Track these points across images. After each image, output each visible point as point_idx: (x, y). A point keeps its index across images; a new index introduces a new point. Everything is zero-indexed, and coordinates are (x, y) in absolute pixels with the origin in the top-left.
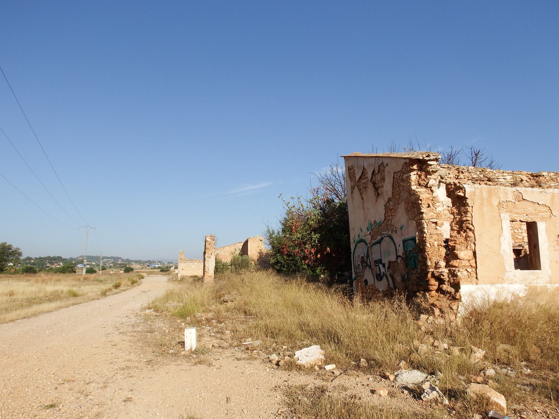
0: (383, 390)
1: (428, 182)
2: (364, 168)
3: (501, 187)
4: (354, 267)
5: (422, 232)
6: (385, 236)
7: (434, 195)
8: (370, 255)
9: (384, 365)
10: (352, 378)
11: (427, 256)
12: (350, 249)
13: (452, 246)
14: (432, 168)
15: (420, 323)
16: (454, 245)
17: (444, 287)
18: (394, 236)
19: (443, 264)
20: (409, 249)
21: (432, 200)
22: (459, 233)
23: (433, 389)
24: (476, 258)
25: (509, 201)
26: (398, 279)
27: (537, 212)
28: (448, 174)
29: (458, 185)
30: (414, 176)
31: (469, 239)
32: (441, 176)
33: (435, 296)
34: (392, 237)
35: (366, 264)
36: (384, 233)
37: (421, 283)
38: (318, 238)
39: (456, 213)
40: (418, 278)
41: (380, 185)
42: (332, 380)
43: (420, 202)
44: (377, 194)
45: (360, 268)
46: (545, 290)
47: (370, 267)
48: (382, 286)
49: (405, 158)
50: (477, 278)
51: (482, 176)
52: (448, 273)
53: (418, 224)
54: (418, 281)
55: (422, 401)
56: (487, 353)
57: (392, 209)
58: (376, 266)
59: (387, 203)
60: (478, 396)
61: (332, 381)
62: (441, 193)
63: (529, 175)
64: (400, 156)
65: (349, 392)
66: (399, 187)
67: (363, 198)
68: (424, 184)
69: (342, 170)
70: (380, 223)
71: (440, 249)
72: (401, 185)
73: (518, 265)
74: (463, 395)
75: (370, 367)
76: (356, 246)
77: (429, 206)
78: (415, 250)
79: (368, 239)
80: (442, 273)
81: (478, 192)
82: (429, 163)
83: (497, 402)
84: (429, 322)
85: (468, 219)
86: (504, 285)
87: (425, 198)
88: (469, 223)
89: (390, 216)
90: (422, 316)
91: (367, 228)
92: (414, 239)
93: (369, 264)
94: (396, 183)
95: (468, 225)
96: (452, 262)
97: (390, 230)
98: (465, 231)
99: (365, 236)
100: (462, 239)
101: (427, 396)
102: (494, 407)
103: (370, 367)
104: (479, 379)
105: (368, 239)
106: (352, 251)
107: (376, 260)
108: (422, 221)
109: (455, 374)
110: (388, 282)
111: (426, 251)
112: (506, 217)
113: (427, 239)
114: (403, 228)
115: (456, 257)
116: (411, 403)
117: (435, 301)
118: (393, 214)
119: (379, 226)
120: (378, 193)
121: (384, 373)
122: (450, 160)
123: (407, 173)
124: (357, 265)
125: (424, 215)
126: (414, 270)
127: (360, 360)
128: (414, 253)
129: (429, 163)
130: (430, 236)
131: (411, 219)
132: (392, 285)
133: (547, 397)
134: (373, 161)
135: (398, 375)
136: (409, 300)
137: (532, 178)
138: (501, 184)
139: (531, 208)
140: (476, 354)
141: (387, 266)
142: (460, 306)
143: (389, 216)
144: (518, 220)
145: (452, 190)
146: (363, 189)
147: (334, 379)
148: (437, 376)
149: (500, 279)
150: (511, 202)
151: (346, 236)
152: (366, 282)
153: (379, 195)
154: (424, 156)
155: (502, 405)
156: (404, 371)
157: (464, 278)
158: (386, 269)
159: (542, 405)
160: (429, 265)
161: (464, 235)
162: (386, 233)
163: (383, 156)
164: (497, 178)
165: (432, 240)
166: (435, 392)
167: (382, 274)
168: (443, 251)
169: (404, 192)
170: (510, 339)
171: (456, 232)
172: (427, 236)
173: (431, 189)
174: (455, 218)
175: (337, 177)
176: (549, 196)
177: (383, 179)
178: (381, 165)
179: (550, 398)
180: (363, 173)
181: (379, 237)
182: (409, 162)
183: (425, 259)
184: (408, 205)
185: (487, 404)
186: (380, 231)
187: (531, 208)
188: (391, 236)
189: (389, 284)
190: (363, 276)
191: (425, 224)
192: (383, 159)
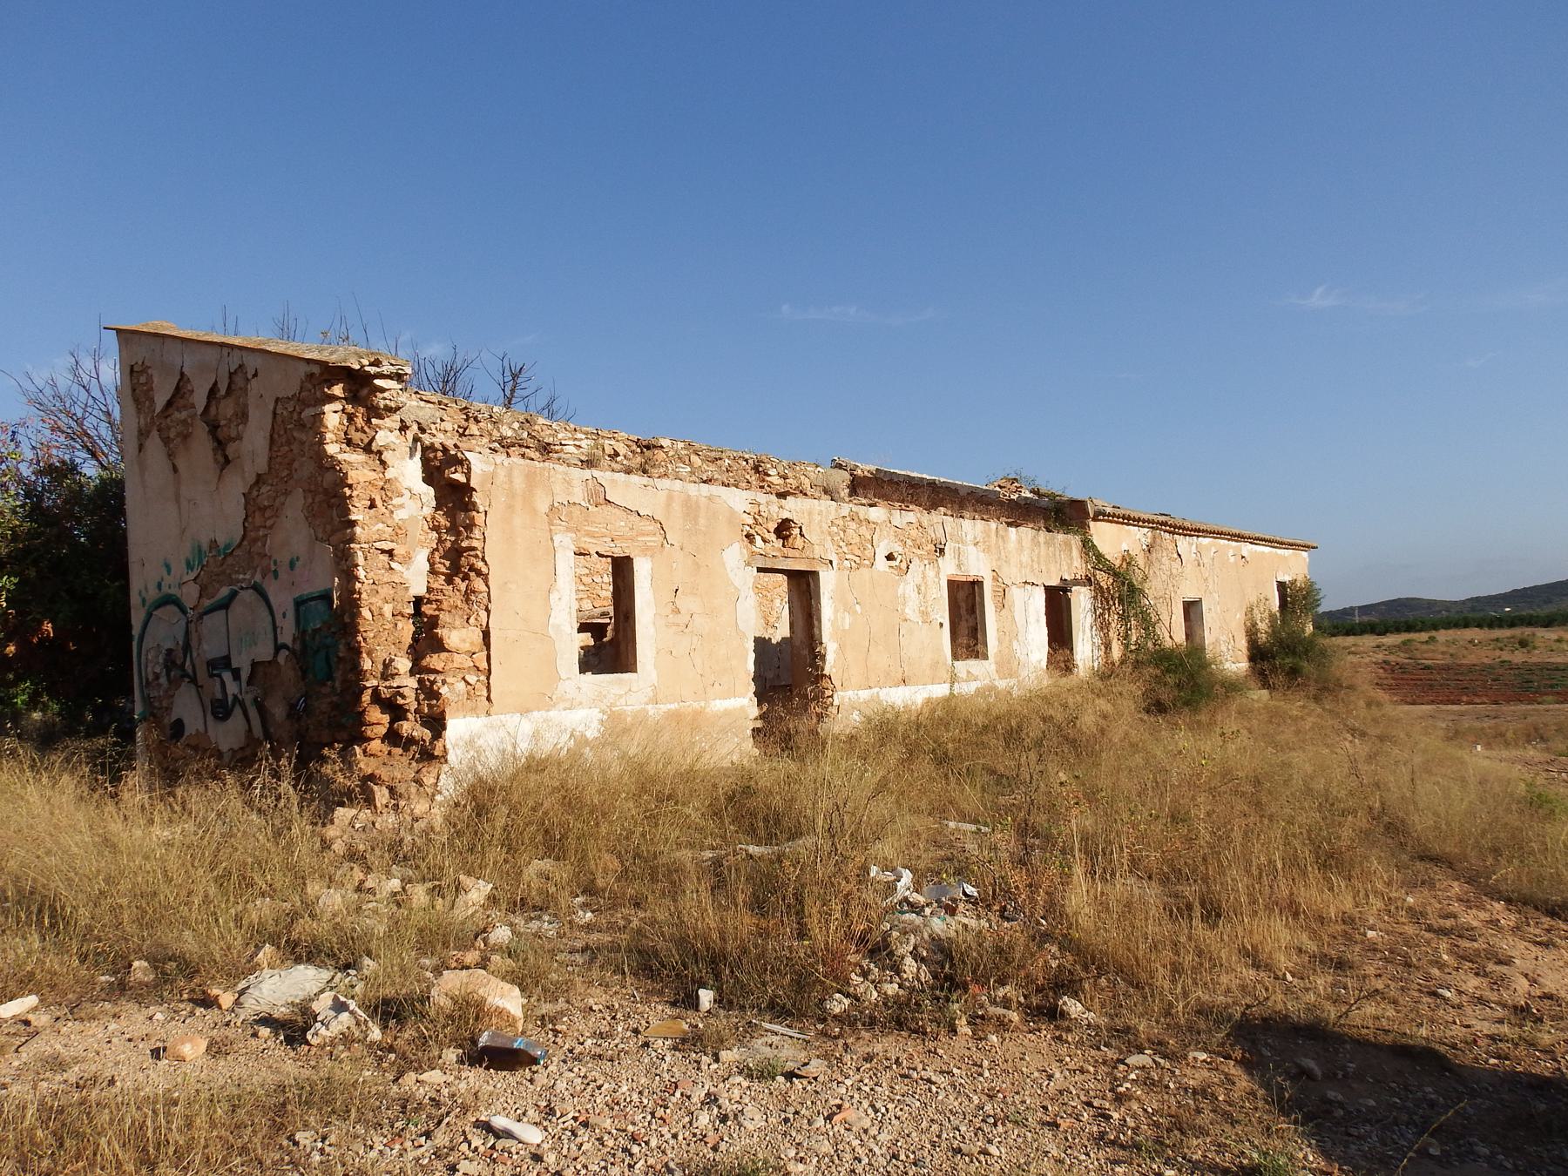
0: (191, 1041)
1: (374, 438)
2: (182, 374)
3: (557, 466)
4: (141, 683)
5: (349, 576)
6: (242, 588)
7: (390, 474)
8: (194, 643)
9: (204, 966)
10: (93, 1028)
11: (363, 644)
12: (130, 627)
13: (431, 616)
14: (385, 399)
15: (331, 832)
16: (437, 613)
17: (405, 727)
18: (272, 589)
19: (403, 664)
20: (311, 627)
21: (382, 489)
22: (449, 581)
23: (339, 1007)
24: (488, 649)
25: (574, 503)
26: (278, 711)
27: (634, 534)
28: (439, 421)
29: (452, 452)
30: (333, 417)
31: (473, 598)
32: (419, 423)
33: (379, 754)
34: (263, 589)
35: (179, 673)
36: (241, 576)
37: (344, 720)
38: (8, 591)
39: (446, 528)
40: (335, 706)
41: (233, 434)
42: (20, 1046)
43: (347, 491)
44: (221, 459)
45: (160, 685)
46: (641, 719)
47: (194, 680)
48: (228, 735)
49: (309, 361)
50: (489, 699)
51: (525, 435)
52: (417, 689)
53: (340, 554)
54: (335, 716)
55: (307, 1048)
56: (497, 888)
57: (266, 508)
58: (212, 676)
59: (251, 488)
60: (456, 1003)
61: (17, 1051)
62: (408, 471)
63: (631, 443)
64: (295, 353)
65: (72, 1075)
66: (289, 443)
67: (175, 469)
68: (362, 440)
69: (110, 373)
70: (228, 546)
71: (400, 625)
72: (295, 439)
73: (599, 663)
74: (419, 1008)
75: (163, 979)
76: (150, 615)
77: (372, 506)
78: (329, 629)
79: (190, 595)
80: (401, 690)
81: (502, 473)
82: (378, 382)
83: (502, 1006)
84: (357, 826)
85: (475, 544)
86: (552, 714)
87: (362, 480)
88: (476, 556)
89: (261, 527)
90: (340, 811)
91: (188, 563)
92: (326, 597)
93: (190, 670)
94: (282, 432)
95: (473, 560)
96: (428, 659)
97: (258, 569)
98: (466, 578)
99: (181, 585)
100: (457, 599)
101: (323, 1031)
102: (494, 1020)
103: (163, 979)
104: (471, 957)
105: (190, 595)
106: (134, 632)
107: (212, 660)
108: (352, 545)
109: (408, 956)
110: (248, 720)
111: (359, 632)
112: (565, 543)
113: (364, 596)
114: (298, 564)
115: (439, 646)
116: (277, 1061)
117: (377, 768)
118: (269, 523)
119: (226, 556)
120: (226, 457)
121: (204, 992)
122: (448, 382)
123: (315, 406)
124: (151, 677)
125: (358, 530)
126: (325, 685)
127: (131, 966)
128: (326, 637)
129: (378, 382)
130: (371, 590)
131: (322, 540)
132: (258, 731)
133: (619, 970)
134: (303, 364)
135: (248, 987)
136: (305, 773)
137: (639, 450)
138: (559, 460)
139: (623, 524)
140: (470, 895)
141: (245, 675)
142: (443, 776)
143: (257, 529)
144: (593, 552)
145: (437, 464)
146: (179, 440)
147: (27, 1041)
148: (362, 969)
149: (546, 700)
150: (578, 507)
151: (117, 584)
152: (178, 727)
153: (227, 461)
154: (365, 362)
155: (512, 1012)
156: (267, 972)
157: (456, 699)
158: (244, 684)
159: (606, 993)
160: (365, 668)
161: (463, 586)
162: (248, 577)
163: (245, 344)
164: (561, 444)
165: (377, 601)
166: (345, 1016)
167: (230, 699)
168: (406, 631)
169: (304, 459)
170: (553, 846)
171: (443, 577)
172: (363, 587)
173: (380, 457)
174: (440, 541)
175: (96, 393)
176: (662, 496)
177: (243, 416)
178: (236, 371)
179: (624, 973)
180: (181, 390)
181: (225, 591)
182: (321, 374)
183: (357, 652)
184: (313, 499)
185: (477, 1018)
186: (228, 571)
187: (623, 524)
188: (260, 586)
189: (250, 730)
190: (169, 709)
191: (360, 553)
192: (244, 354)
